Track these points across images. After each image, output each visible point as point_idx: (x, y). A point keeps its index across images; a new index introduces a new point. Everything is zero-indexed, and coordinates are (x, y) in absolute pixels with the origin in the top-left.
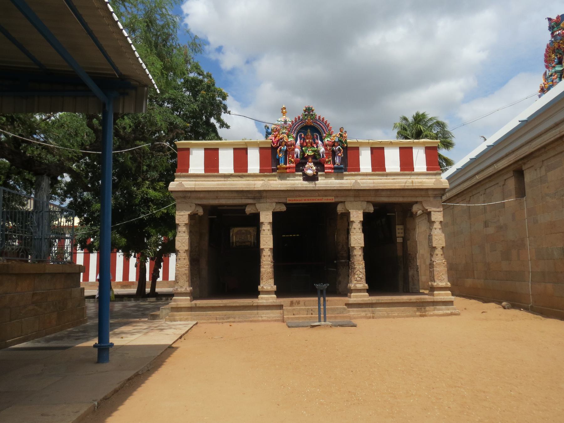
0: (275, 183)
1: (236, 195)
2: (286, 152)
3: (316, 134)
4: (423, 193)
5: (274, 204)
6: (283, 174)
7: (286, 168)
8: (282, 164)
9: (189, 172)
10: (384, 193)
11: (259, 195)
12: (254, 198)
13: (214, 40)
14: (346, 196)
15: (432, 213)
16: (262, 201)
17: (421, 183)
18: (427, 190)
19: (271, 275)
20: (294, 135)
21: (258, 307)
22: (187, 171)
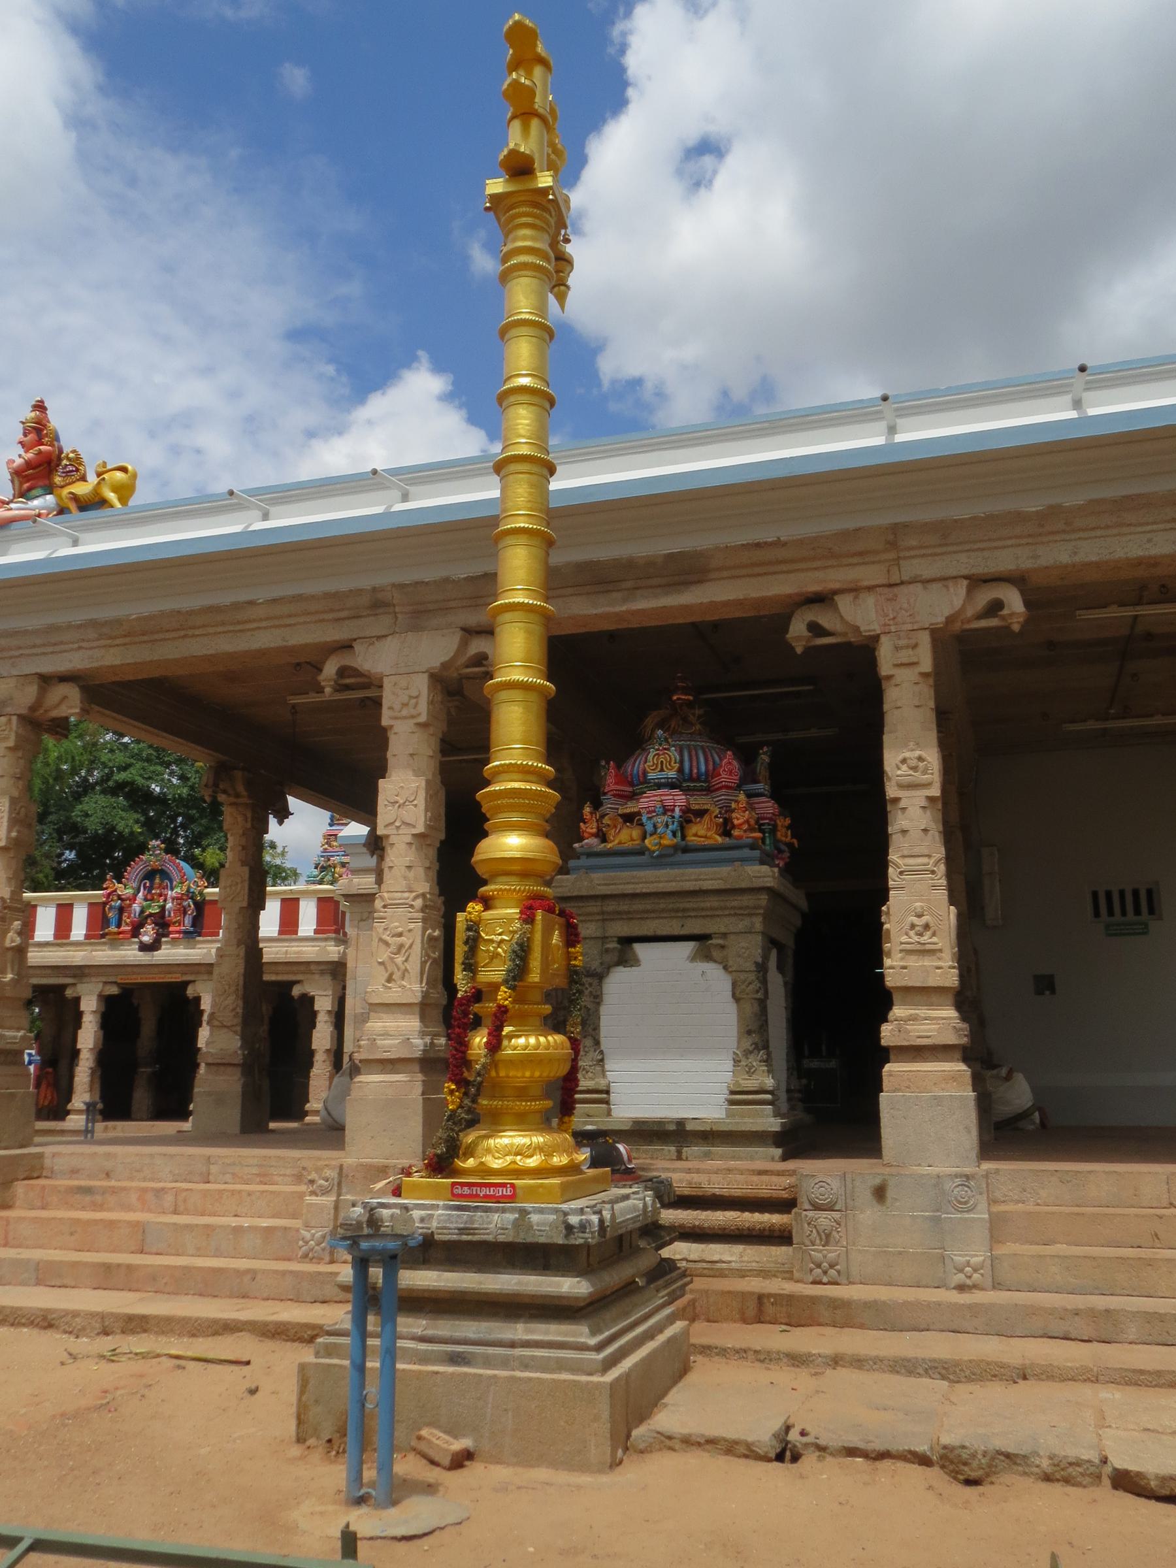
0: (104, 955)
1: (49, 971)
2: (121, 910)
3: (167, 882)
4: (302, 968)
5: (101, 985)
6: (115, 941)
7: (120, 933)
8: (113, 928)
9: (300, 934)
10: (280, 968)
11: (81, 972)
12: (74, 976)
13: (440, 735)
14: (198, 973)
15: (316, 998)
16: (85, 980)
17: (298, 952)
18: (308, 963)
19: (87, 1087)
20: (135, 885)
21: (62, 1132)
22: (68, 937)
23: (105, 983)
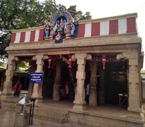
5: (43, 56)
11: (36, 51)
23: (44, 55)
